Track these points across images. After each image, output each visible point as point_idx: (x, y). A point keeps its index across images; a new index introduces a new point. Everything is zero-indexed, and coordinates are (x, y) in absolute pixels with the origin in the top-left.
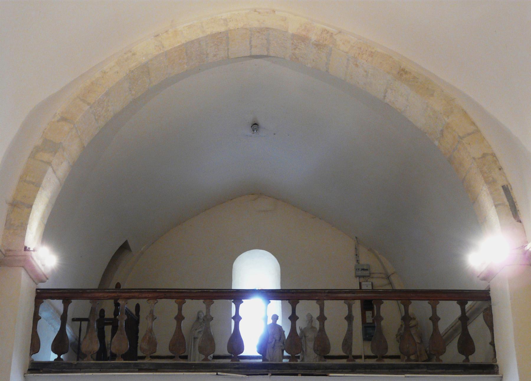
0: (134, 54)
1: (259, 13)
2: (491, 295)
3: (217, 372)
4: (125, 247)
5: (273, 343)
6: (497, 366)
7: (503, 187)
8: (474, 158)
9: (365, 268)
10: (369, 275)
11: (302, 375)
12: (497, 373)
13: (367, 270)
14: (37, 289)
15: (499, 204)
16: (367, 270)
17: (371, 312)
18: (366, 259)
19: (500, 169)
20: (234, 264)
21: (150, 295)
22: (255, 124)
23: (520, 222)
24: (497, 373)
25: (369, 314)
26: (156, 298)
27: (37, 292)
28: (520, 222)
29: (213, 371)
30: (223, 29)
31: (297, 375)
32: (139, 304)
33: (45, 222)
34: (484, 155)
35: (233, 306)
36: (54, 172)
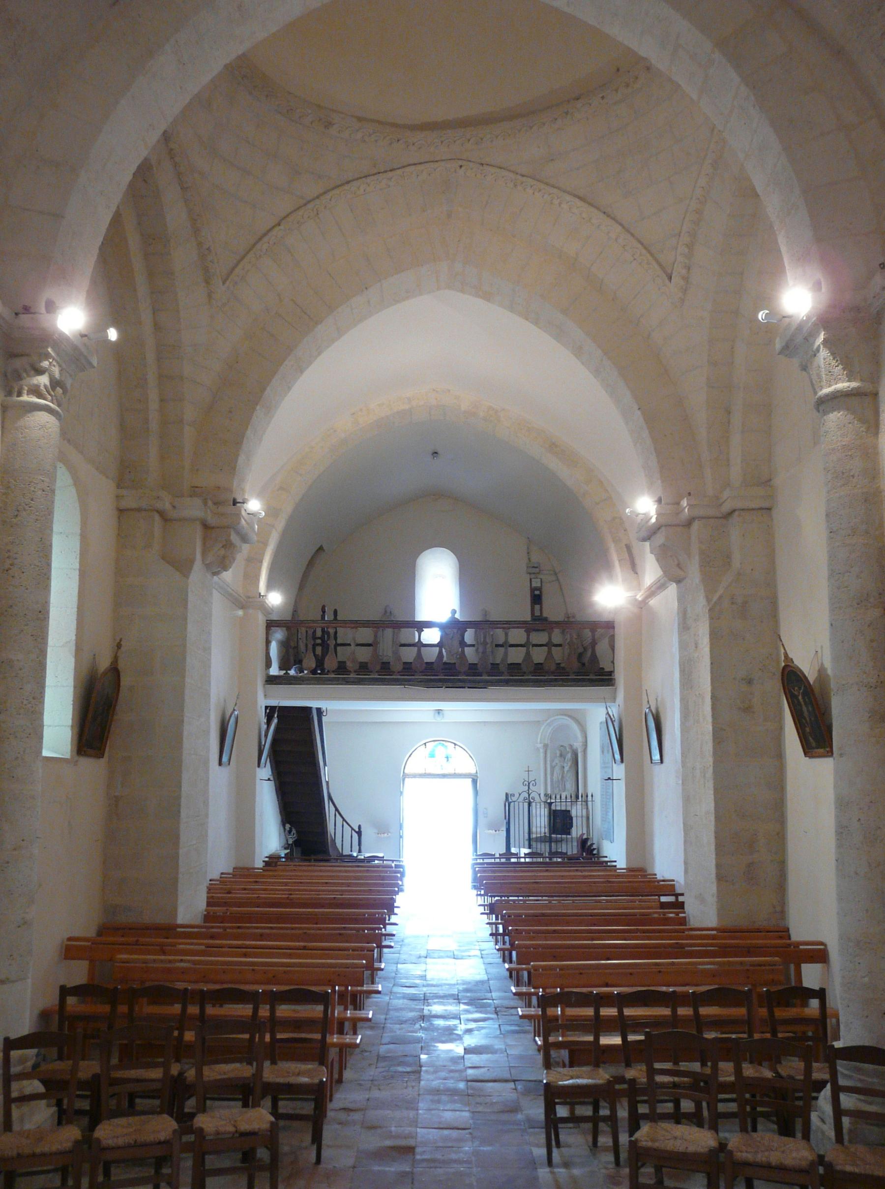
0: (335, 431)
1: (437, 392)
2: (615, 625)
3: (404, 685)
4: (321, 549)
5: (452, 635)
6: (615, 679)
7: (626, 545)
8: (605, 521)
9: (535, 566)
10: (538, 572)
11: (469, 688)
12: (613, 685)
13: (537, 567)
14: (267, 620)
15: (622, 560)
16: (537, 567)
17: (539, 606)
18: (535, 558)
19: (625, 530)
20: (418, 560)
21: (353, 625)
22: (436, 453)
23: (637, 574)
24: (613, 685)
25: (537, 607)
26: (356, 628)
27: (267, 623)
28: (637, 574)
29: (446, 1109)
30: (407, 407)
31: (464, 688)
32: (338, 610)
33: (269, 567)
34: (614, 519)
35: (417, 634)
36: (276, 530)
